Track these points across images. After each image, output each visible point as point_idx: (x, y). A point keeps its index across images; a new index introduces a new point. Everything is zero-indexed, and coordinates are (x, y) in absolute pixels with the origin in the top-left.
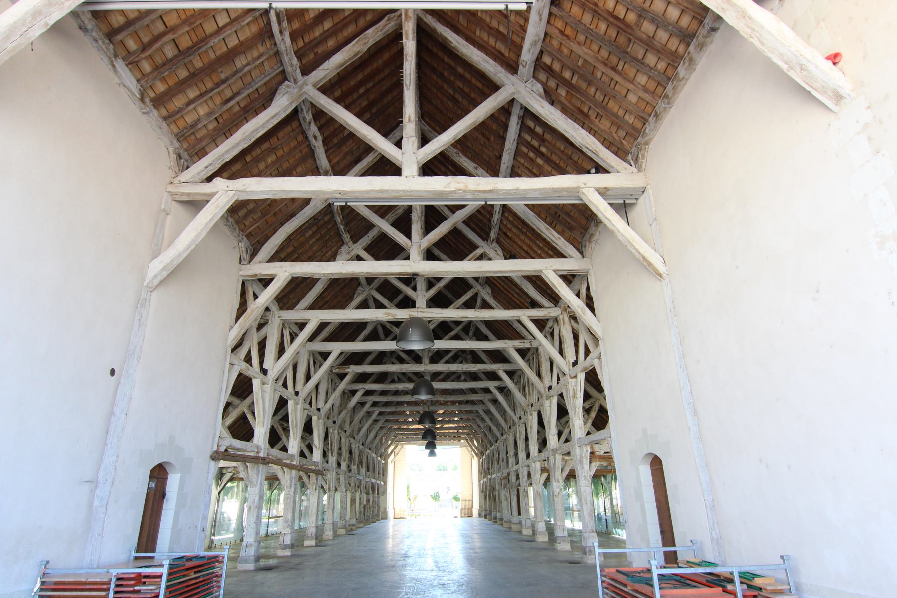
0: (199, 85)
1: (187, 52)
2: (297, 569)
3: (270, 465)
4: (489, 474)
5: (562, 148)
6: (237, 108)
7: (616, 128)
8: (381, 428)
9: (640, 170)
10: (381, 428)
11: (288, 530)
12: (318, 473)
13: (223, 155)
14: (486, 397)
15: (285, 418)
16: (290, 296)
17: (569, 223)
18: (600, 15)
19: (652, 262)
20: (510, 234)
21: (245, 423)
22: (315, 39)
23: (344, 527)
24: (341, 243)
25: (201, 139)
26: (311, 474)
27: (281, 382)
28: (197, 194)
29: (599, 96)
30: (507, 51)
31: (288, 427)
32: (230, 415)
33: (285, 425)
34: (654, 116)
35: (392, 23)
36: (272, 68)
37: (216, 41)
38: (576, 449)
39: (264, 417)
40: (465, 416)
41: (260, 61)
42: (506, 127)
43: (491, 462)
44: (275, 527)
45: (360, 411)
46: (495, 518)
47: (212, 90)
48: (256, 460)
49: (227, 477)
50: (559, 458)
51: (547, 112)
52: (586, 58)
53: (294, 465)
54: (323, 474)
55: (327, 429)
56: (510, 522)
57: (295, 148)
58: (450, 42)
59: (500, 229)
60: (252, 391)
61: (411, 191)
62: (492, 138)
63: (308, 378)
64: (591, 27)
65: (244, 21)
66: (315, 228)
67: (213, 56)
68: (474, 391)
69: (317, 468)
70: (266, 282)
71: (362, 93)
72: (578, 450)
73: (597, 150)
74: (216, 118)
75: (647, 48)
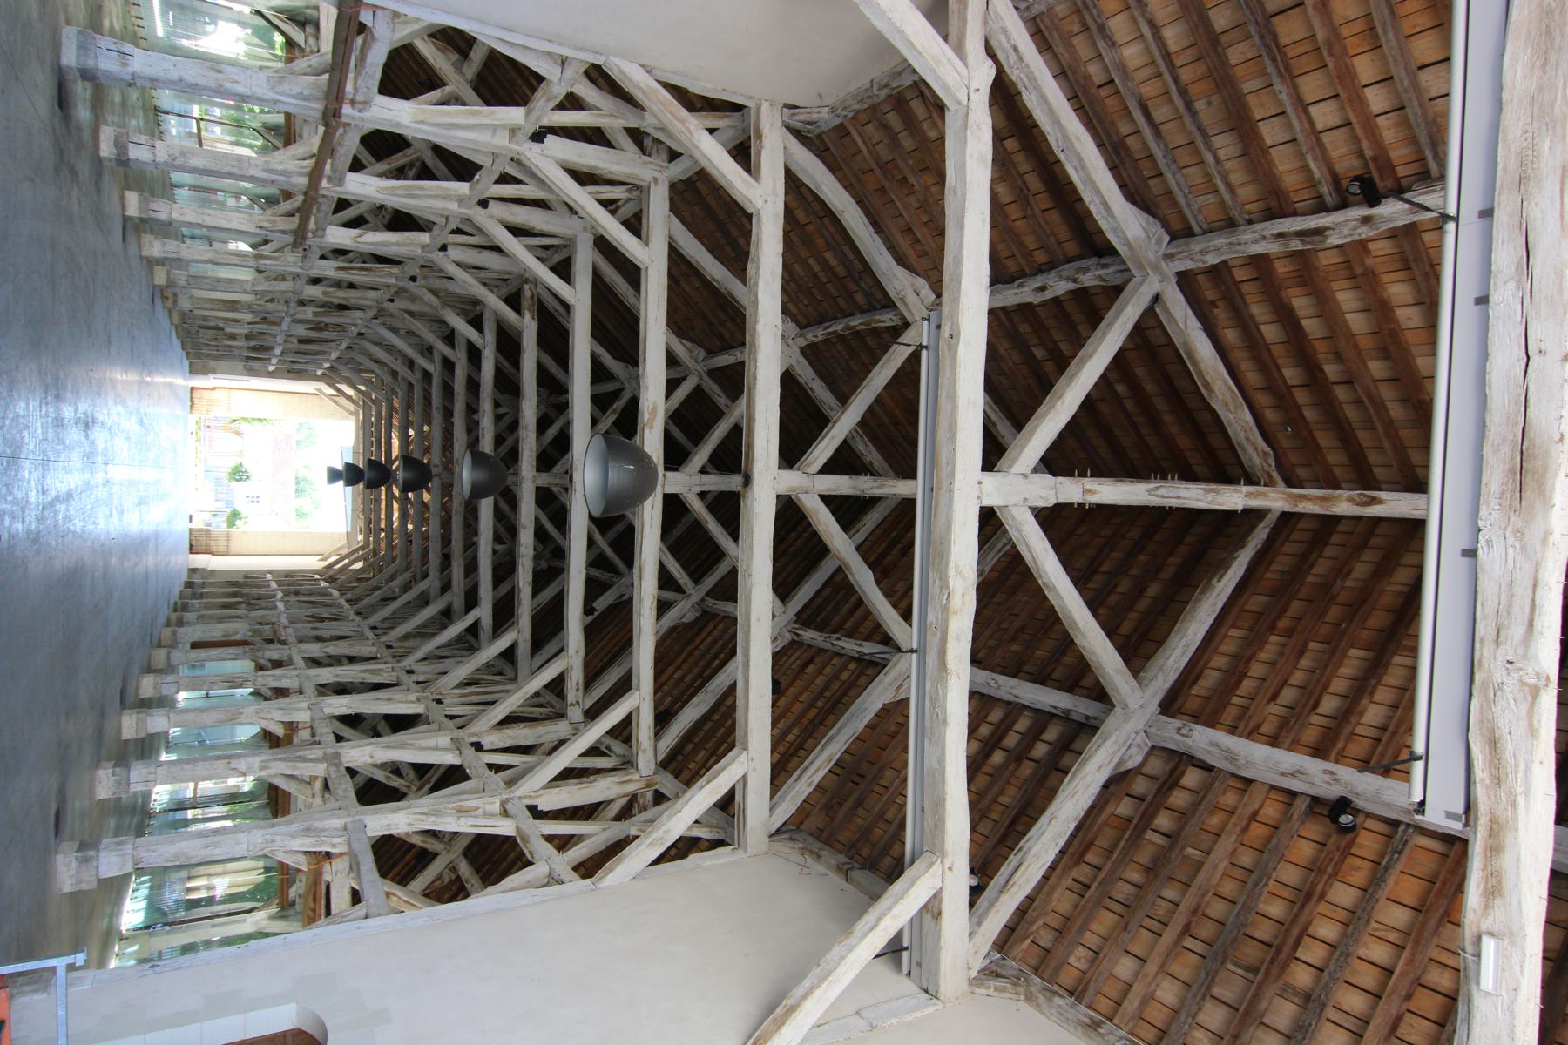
0: (1189, 52)
1: (1269, 31)
2: (57, 169)
3: (321, 129)
4: (287, 594)
5: (1004, 799)
6: (1124, 128)
7: (1055, 925)
8: (394, 374)
9: (975, 982)
10: (394, 374)
11: (162, 155)
12: (299, 237)
13: (1038, 88)
14: (456, 597)
15: (426, 173)
16: (697, 208)
17: (841, 805)
18: (1303, 906)
19: (784, 1029)
20: (810, 669)
21: (421, 84)
22: (1247, 306)
23: (171, 284)
24: (804, 322)
25: (1069, 46)
26: (296, 220)
27: (512, 171)
28: (964, 20)
29: (1123, 891)
30: (1203, 693)
31: (405, 179)
32: (439, 54)
33: (411, 173)
34: (1091, 1019)
35: (1257, 461)
36: (1200, 211)
37: (1283, 97)
38: (339, 817)
39: (437, 125)
40: (415, 548)
41: (1222, 187)
42: (1041, 679)
43: (312, 599)
44: (179, 132)
45: (433, 332)
46: (185, 608)
47: (1176, 79)
48: (334, 98)
49: (298, 36)
50: (320, 770)
51: (1089, 779)
52: (1206, 867)
53: (319, 181)
54: (295, 245)
55: (399, 263)
56: (173, 645)
57: (1022, 245)
58: (1221, 578)
59: (821, 650)
60: (488, 104)
61: (951, 491)
62: (1015, 647)
63: (517, 231)
64: (1271, 882)
65: (1315, 159)
66: (841, 271)
67: (1247, 87)
68: (471, 567)
69: (310, 235)
70: (743, 153)
71: (1115, 391)
72: (337, 823)
73: (1015, 888)
74: (1112, 81)
75: (1242, 1010)
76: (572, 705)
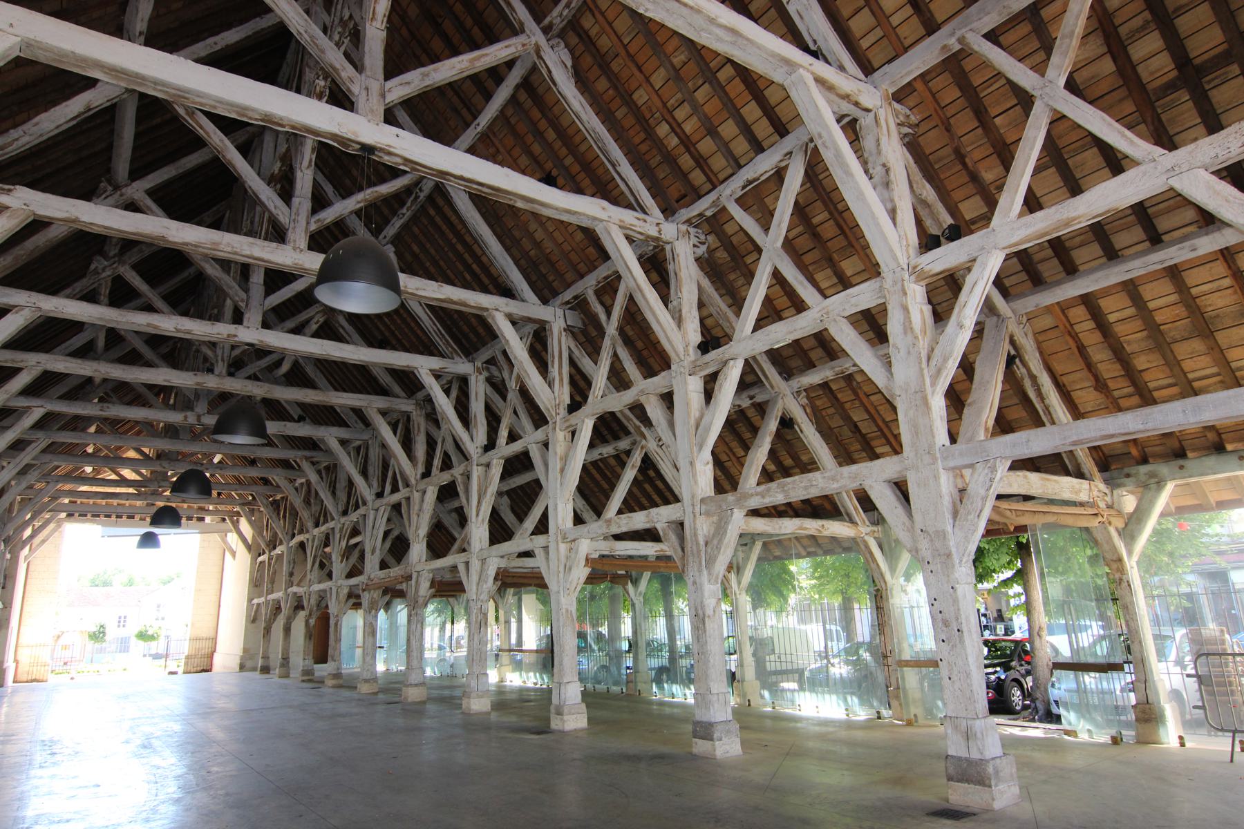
76: (659, 232)
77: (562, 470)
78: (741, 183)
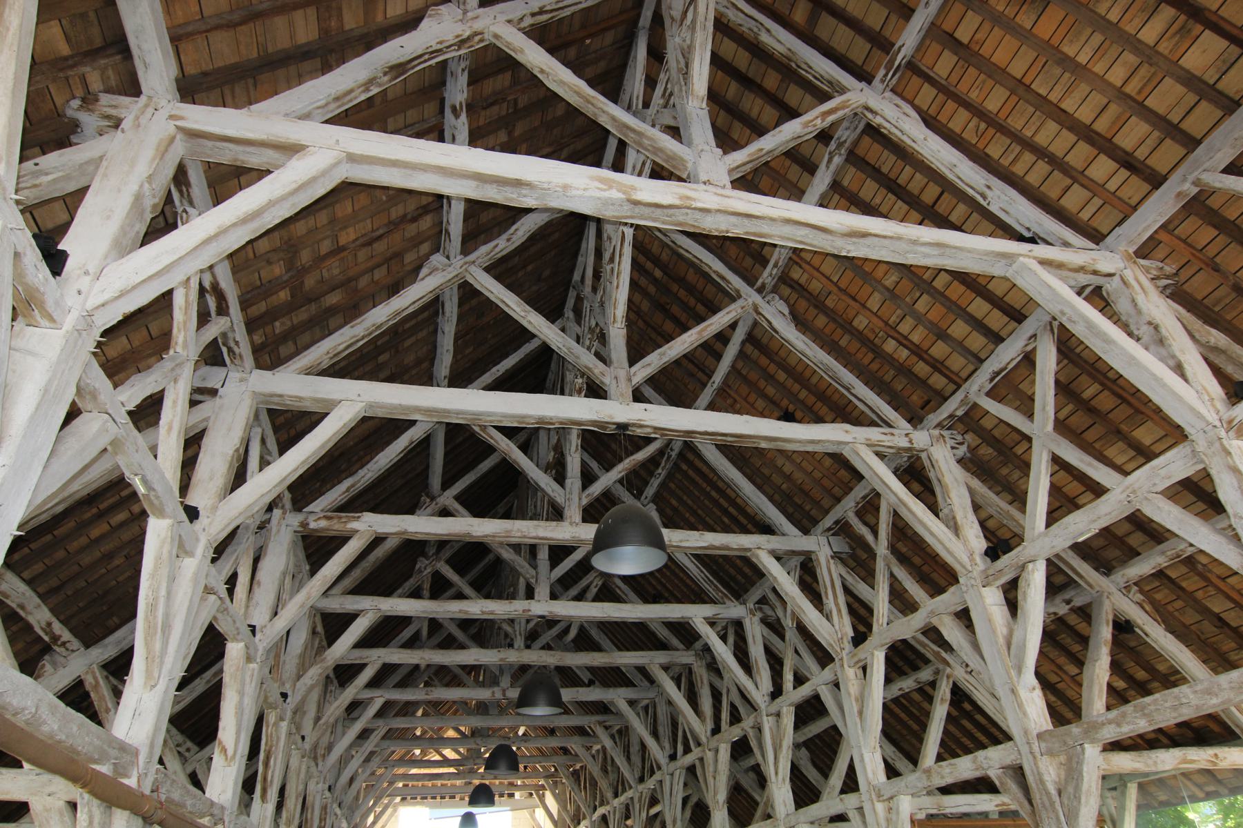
76: (911, 442)
77: (861, 713)
78: (988, 376)
